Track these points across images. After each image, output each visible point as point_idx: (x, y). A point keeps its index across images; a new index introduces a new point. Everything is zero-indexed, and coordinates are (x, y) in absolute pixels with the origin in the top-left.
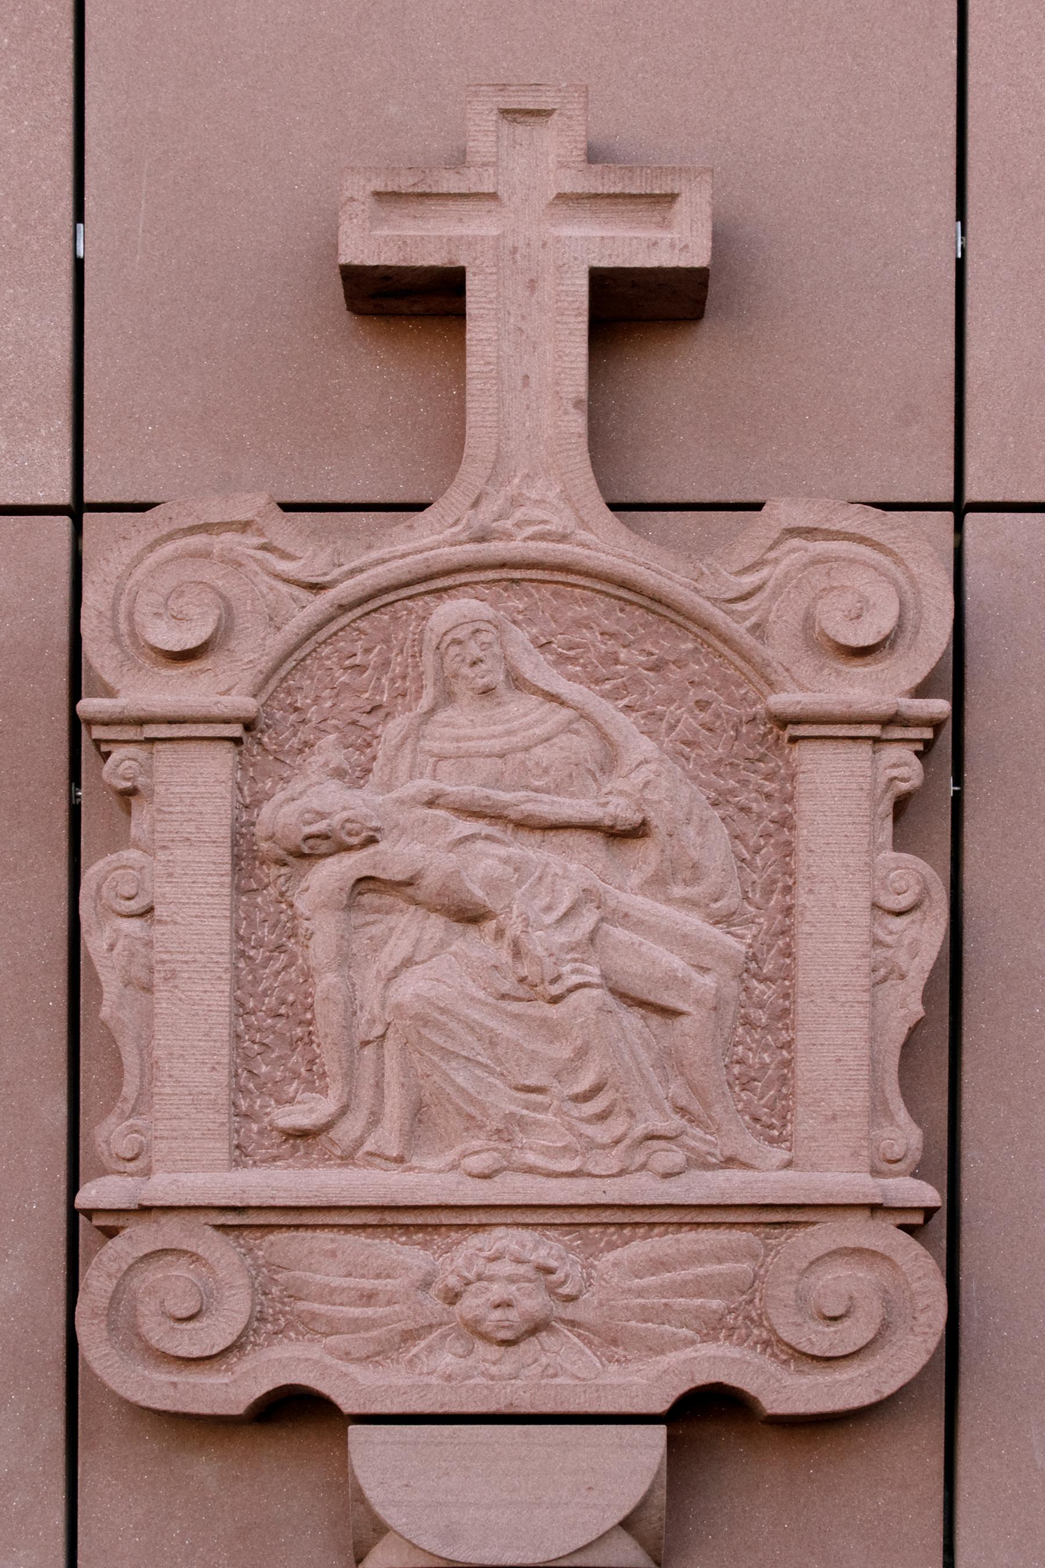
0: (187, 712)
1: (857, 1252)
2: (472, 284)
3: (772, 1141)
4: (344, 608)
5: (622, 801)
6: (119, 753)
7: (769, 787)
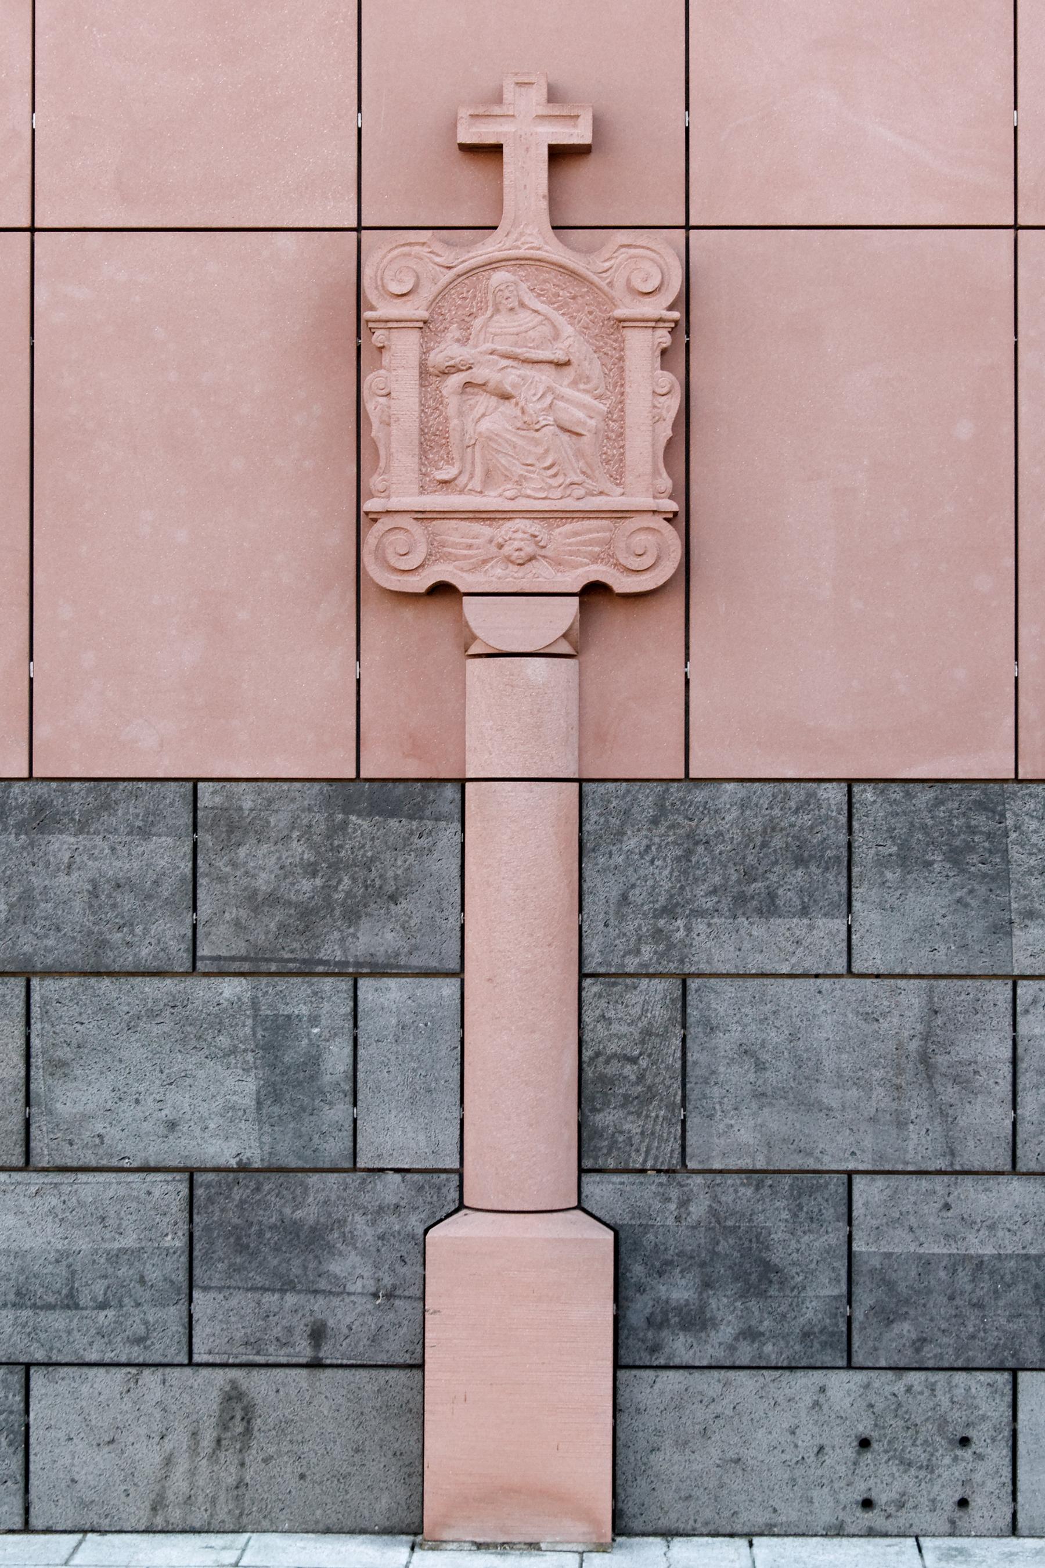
0: (403, 318)
1: (648, 528)
2: (505, 150)
3: (617, 485)
4: (459, 276)
5: (561, 352)
6: (378, 333)
7: (615, 345)
